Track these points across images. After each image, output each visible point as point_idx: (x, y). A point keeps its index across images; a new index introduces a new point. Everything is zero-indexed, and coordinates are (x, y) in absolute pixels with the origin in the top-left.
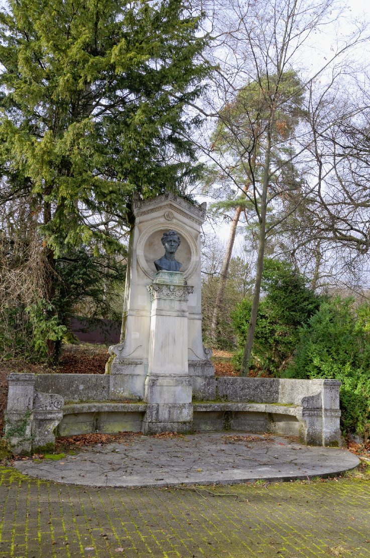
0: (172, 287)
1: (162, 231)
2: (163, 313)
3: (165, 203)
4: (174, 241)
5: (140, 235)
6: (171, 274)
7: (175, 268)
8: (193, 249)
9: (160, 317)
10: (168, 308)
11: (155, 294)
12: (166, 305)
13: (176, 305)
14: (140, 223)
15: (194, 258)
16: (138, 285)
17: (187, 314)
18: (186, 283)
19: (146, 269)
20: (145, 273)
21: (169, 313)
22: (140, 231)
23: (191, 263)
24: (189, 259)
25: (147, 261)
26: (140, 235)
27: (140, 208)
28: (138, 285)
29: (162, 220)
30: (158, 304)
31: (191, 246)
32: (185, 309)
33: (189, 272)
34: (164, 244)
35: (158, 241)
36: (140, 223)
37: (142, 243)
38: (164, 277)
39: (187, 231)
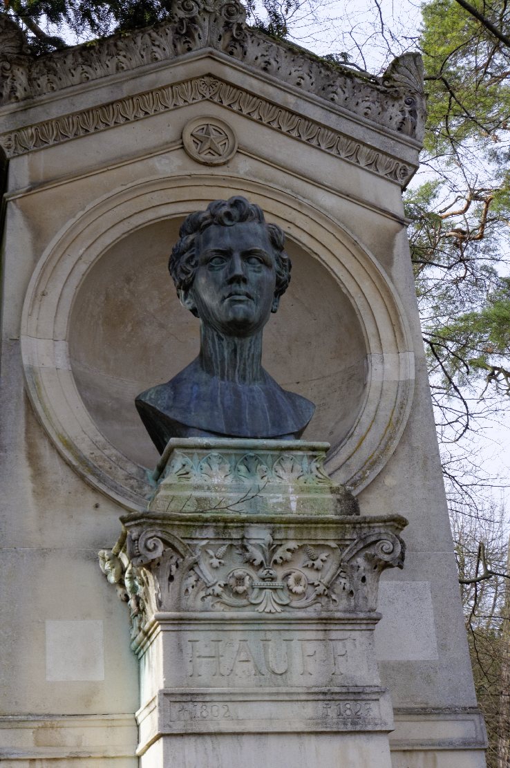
0: (259, 536)
1: (161, 225)
2: (217, 717)
3: (180, 72)
4: (247, 255)
5: (37, 252)
6: (249, 459)
7: (269, 423)
8: (376, 323)
9: (191, 750)
10: (244, 679)
11: (153, 589)
12: (230, 659)
13: (302, 658)
14: (37, 185)
15: (385, 369)
16: (43, 552)
17: (381, 711)
18: (350, 503)
19: (85, 449)
20: (85, 473)
21: (255, 716)
22: (39, 235)
23: (372, 393)
24: (357, 377)
25: (98, 410)
26: (37, 252)
27: (29, 102)
28: (43, 552)
29: (172, 164)
30: (175, 656)
31: (358, 302)
32: (368, 676)
33: (365, 452)
34: (187, 287)
35: (156, 292)
36: (37, 185)
37: (53, 297)
38: (205, 479)
39: (322, 216)
